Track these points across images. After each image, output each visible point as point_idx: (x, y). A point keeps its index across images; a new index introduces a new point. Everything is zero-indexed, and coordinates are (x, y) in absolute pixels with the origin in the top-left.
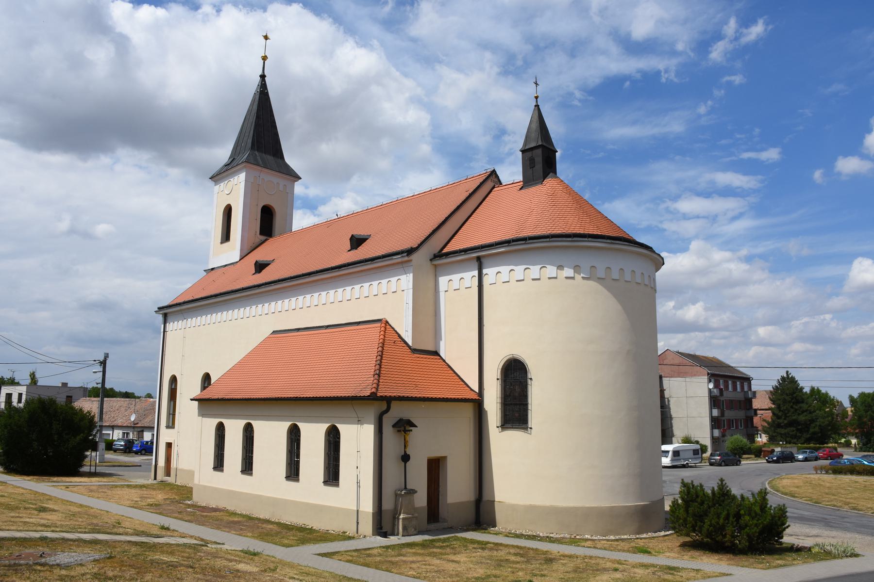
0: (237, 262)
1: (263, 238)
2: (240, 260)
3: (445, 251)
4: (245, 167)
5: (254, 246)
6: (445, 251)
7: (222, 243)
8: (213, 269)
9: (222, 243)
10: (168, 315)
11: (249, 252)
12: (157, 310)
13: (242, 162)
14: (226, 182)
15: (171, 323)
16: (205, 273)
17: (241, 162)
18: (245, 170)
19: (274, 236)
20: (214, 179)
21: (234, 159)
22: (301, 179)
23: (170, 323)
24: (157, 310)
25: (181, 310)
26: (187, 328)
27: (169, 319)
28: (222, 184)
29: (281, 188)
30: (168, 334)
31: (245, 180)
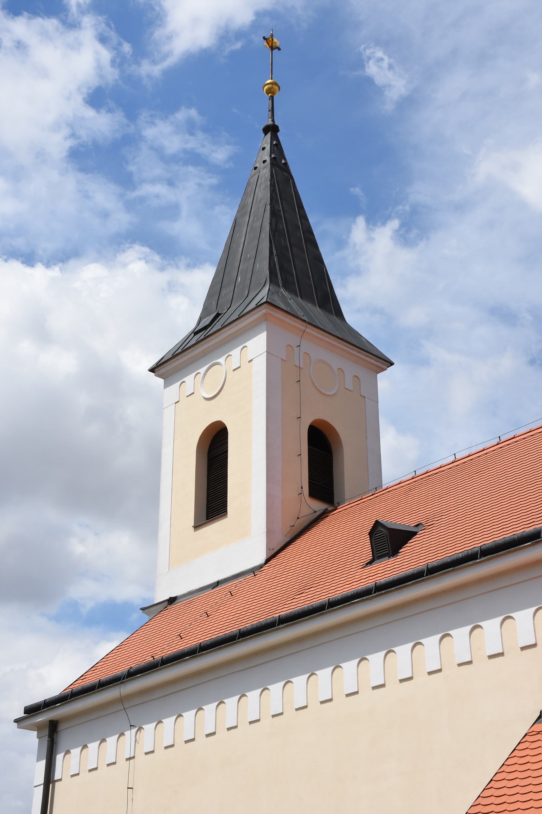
0: (261, 566)
1: (319, 506)
2: (267, 561)
3: (521, 742)
4: (265, 318)
5: (304, 521)
6: (521, 742)
7: (197, 527)
8: (172, 601)
9: (197, 527)
10: (61, 727)
11: (288, 539)
12: (22, 714)
13: (258, 306)
14: (202, 370)
15: (75, 752)
16: (146, 618)
17: (253, 305)
18: (264, 326)
19: (343, 501)
20: (162, 370)
21: (218, 315)
22: (392, 364)
23: (68, 752)
24: (22, 714)
25: (121, 700)
26: (140, 757)
27: (63, 739)
28: (189, 379)
29: (349, 383)
30: (59, 789)
31: (267, 352)
